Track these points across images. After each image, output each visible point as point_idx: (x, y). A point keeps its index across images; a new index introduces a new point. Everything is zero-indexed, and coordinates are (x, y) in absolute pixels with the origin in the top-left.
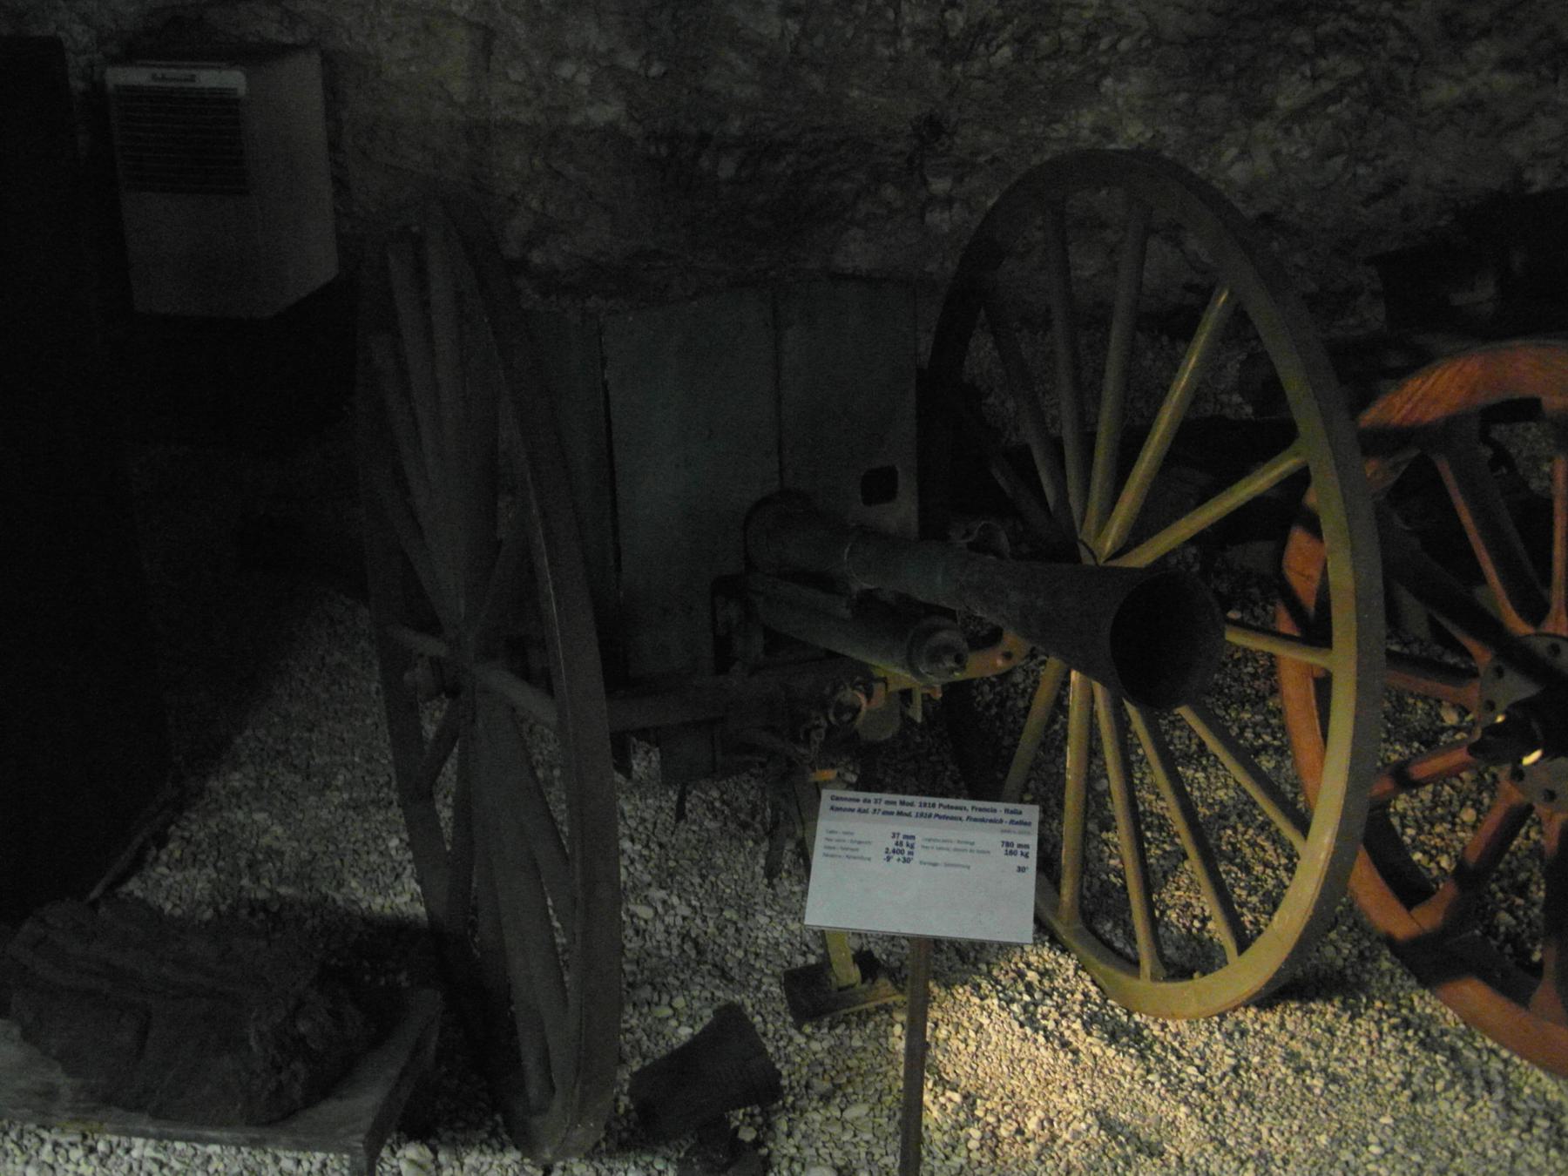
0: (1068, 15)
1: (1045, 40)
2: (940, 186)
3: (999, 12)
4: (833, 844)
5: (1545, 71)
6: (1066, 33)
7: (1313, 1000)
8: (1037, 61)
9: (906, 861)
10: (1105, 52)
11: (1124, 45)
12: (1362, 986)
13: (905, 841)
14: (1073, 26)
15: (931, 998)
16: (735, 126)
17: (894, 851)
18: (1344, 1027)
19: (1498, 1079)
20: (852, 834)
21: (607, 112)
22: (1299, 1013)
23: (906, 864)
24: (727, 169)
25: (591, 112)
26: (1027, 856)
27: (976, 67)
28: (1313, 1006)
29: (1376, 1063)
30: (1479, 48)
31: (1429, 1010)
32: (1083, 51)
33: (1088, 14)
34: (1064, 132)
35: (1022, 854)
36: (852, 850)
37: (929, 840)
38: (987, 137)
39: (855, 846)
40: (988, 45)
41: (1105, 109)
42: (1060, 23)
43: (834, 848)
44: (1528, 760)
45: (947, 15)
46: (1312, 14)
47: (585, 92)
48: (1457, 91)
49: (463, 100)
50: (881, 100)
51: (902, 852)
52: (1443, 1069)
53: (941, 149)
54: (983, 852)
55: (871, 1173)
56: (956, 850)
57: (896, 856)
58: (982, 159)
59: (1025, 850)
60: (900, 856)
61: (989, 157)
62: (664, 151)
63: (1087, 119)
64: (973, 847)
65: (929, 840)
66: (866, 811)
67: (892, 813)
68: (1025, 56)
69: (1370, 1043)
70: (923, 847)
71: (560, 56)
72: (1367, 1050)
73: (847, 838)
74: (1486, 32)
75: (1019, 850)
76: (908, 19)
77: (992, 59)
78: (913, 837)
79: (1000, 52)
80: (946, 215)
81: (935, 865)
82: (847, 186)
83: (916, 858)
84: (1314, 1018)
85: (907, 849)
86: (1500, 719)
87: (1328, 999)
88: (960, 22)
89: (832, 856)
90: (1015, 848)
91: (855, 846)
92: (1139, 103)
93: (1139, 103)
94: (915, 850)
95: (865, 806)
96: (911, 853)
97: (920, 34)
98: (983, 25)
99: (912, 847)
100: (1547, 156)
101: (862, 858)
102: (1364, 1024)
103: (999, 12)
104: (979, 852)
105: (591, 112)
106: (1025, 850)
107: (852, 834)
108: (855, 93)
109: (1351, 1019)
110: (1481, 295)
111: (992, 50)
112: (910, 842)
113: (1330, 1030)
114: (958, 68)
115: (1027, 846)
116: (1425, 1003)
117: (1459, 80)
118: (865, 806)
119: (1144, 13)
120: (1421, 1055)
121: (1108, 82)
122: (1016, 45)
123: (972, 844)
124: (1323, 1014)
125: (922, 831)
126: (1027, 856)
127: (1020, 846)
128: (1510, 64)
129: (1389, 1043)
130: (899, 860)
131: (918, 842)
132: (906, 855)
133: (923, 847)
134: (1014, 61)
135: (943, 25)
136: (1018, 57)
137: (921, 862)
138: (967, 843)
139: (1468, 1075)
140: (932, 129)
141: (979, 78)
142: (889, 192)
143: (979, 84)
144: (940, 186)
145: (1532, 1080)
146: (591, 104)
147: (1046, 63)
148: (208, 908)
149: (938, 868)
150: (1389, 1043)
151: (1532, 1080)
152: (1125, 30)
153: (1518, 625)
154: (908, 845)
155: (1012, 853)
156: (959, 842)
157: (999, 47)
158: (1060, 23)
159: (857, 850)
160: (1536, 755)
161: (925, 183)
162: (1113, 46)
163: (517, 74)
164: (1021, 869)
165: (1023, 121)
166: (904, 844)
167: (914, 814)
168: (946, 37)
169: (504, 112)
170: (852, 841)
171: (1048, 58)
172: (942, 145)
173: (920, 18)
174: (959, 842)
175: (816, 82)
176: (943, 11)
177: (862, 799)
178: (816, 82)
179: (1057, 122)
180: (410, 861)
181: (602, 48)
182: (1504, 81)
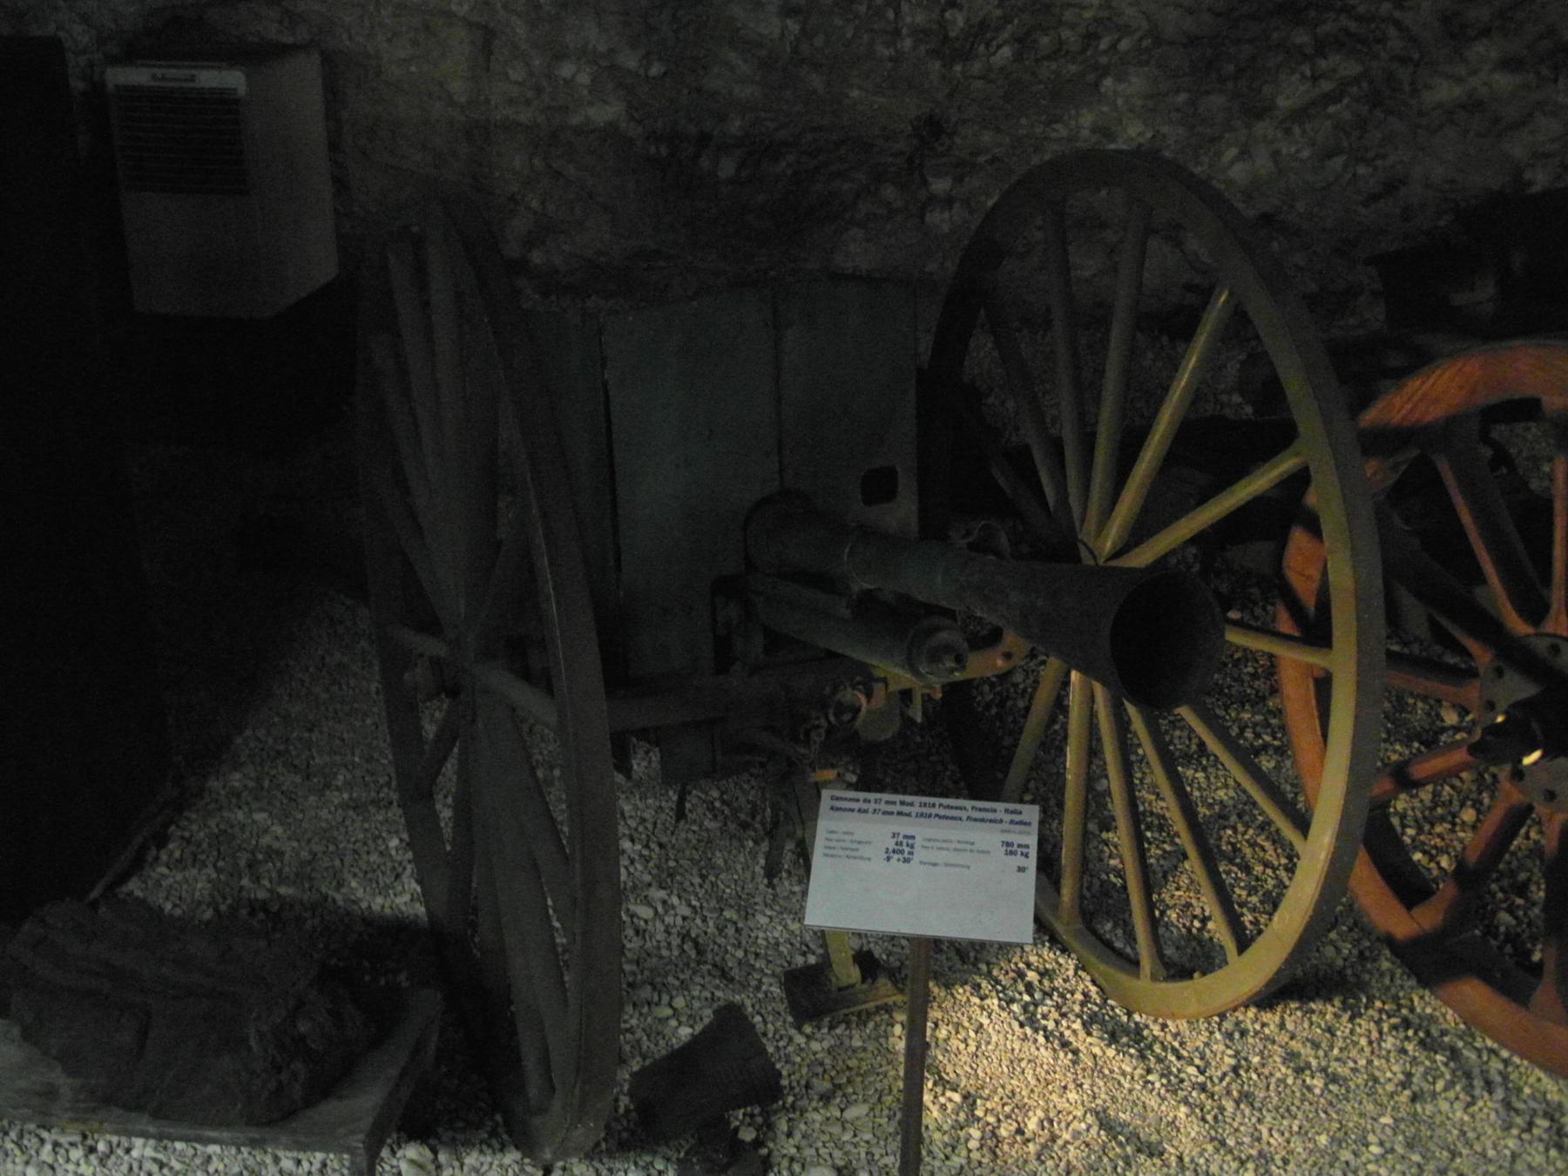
0: (1068, 15)
1: (1045, 40)
2: (940, 186)
3: (999, 12)
4: (833, 844)
5: (1545, 71)
6: (1066, 33)
7: (1313, 1000)
8: (1037, 61)
9: (906, 861)
10: (1105, 52)
11: (1124, 45)
12: (1362, 986)
13: (905, 841)
14: (1073, 26)
15: (931, 998)
16: (735, 126)
17: (894, 851)
18: (1344, 1027)
19: (1498, 1079)
20: (852, 834)
21: (607, 112)
22: (1299, 1013)
23: (906, 864)
24: (727, 169)
25: (591, 112)
26: (1027, 856)
27: (976, 67)
28: (1313, 1006)
29: (1376, 1063)
30: (1479, 48)
31: (1429, 1010)
32: (1083, 51)
33: (1088, 14)
34: (1064, 132)
35: (1022, 854)
36: (852, 850)
37: (929, 840)
38: (987, 137)
39: (855, 846)
40: (988, 45)
41: (1105, 109)
42: (1060, 23)
43: (834, 848)
44: (1528, 760)
45: (947, 15)
46: (1312, 14)
47: (585, 92)
48: (1457, 91)
49: (463, 100)
50: (881, 100)
51: (902, 852)
52: (1443, 1069)
53: (941, 149)
54: (983, 852)
55: (871, 1173)
56: (956, 850)
57: (896, 856)
58: (982, 159)
59: (1025, 850)
60: (900, 856)
61: (989, 157)
62: (664, 151)
63: (1087, 119)
64: (973, 847)
65: (929, 840)
66: (866, 811)
67: (892, 813)
68: (1025, 56)
69: (1370, 1043)
70: (923, 847)
71: (560, 56)
72: (1367, 1050)
73: (847, 838)
74: (1486, 32)
75: (1019, 850)
76: (908, 19)
77: (992, 59)
78: (913, 837)
79: (1000, 52)
80: (946, 215)
81: (935, 865)
82: (847, 186)
83: (916, 858)
84: (1314, 1018)
85: (907, 849)
86: (1500, 719)
87: (1328, 999)
88: (960, 22)
89: (832, 856)
90: (1015, 848)
91: (855, 846)
92: (1139, 103)
93: (1139, 103)
94: (915, 850)
95: (865, 806)
96: (911, 853)
97: (920, 34)
98: (983, 25)
99: (912, 847)
100: (1547, 156)
101: (862, 858)
102: (1364, 1024)
103: (999, 12)
104: (979, 852)
105: (591, 112)
106: (1025, 850)
107: (852, 834)
108: (855, 93)
109: (1351, 1019)
110: (1481, 295)
111: (992, 50)
112: (910, 842)
113: (1330, 1030)
114: (958, 68)
115: (1027, 846)
116: (1425, 1003)
117: (1459, 80)
118: (865, 806)
119: (1144, 13)
120: (1421, 1055)
121: (1108, 82)
122: (1016, 45)
123: (972, 844)
124: (1323, 1014)
125: (922, 831)
126: (1027, 856)
127: (1020, 846)
128: (1510, 64)
129: (1389, 1043)
130: (899, 860)
131: (918, 842)
132: (906, 855)
133: (923, 847)
134: (1014, 61)
135: (943, 25)
136: (1018, 57)
137: (921, 862)
138: (967, 843)
139: (1468, 1075)
140: (932, 129)
141: (979, 78)
142: (889, 192)
143: (979, 84)
144: (940, 186)
145: (1532, 1080)
146: (591, 104)
147: (1046, 63)
148: (208, 908)
149: (938, 868)
150: (1389, 1043)
151: (1532, 1080)
152: (1125, 30)
153: (1518, 625)
154: (908, 845)
155: (1012, 853)
156: (959, 842)
157: (999, 47)
158: (1060, 23)
159: (857, 850)
160: (1536, 755)
161: (925, 183)
162: (1113, 46)
163: (517, 74)
164: (1021, 869)
165: (1023, 121)
166: (904, 844)
167: (914, 814)
168: (946, 37)
169: (504, 112)
170: (852, 841)
171: (1048, 58)
172: (942, 145)
173: (920, 18)
174: (959, 842)
175: (816, 82)
176: (943, 11)
177: (862, 799)
178: (816, 82)
179: (1057, 122)
180: (410, 861)
181: (602, 48)
182: (1504, 81)
